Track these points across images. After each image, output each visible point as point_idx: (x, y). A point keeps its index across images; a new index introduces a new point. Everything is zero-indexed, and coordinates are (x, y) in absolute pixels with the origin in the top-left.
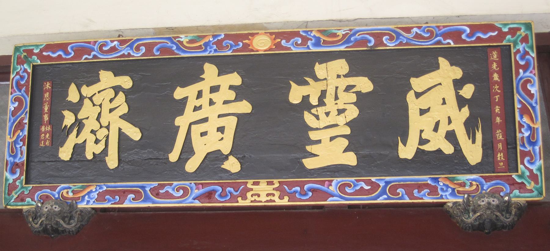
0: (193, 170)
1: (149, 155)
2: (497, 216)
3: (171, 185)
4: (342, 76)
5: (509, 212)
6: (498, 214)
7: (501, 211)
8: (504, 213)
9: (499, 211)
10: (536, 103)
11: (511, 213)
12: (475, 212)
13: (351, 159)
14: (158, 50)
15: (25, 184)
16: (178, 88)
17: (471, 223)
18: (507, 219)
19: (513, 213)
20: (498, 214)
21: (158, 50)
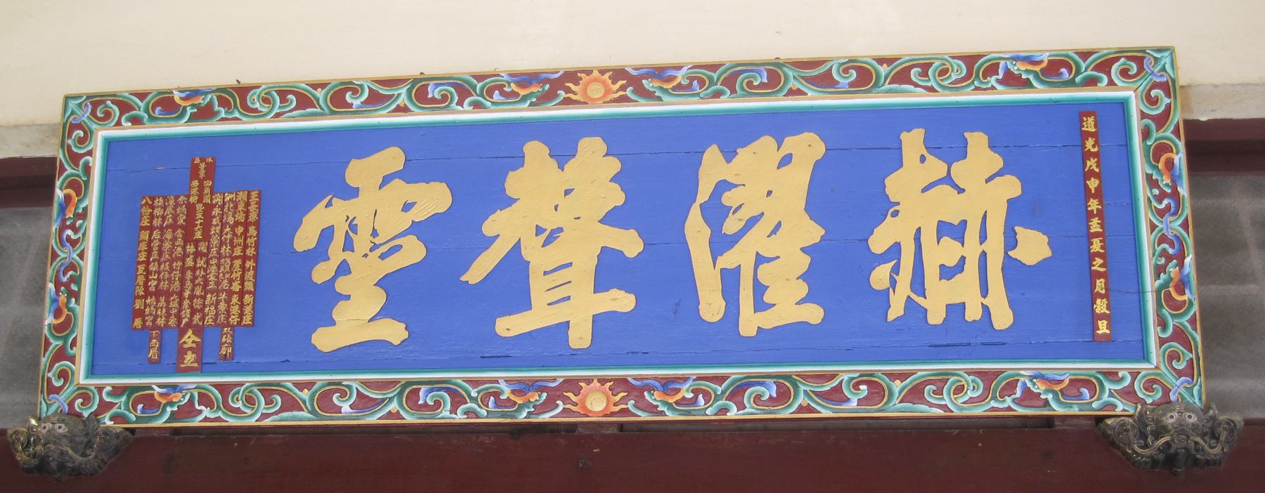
0: (586, 343)
1: (446, 294)
2: (1196, 443)
3: (206, 419)
4: (984, 247)
5: (1214, 436)
6: (1198, 439)
7: (1203, 436)
8: (1207, 438)
9: (1198, 435)
10: (903, 376)
11: (1218, 439)
12: (1157, 435)
13: (394, 332)
14: (1122, 379)
15: (87, 377)
16: (823, 232)
17: (1151, 457)
18: (1215, 451)
19: (1223, 438)
20: (1198, 439)
21: (1122, 379)
